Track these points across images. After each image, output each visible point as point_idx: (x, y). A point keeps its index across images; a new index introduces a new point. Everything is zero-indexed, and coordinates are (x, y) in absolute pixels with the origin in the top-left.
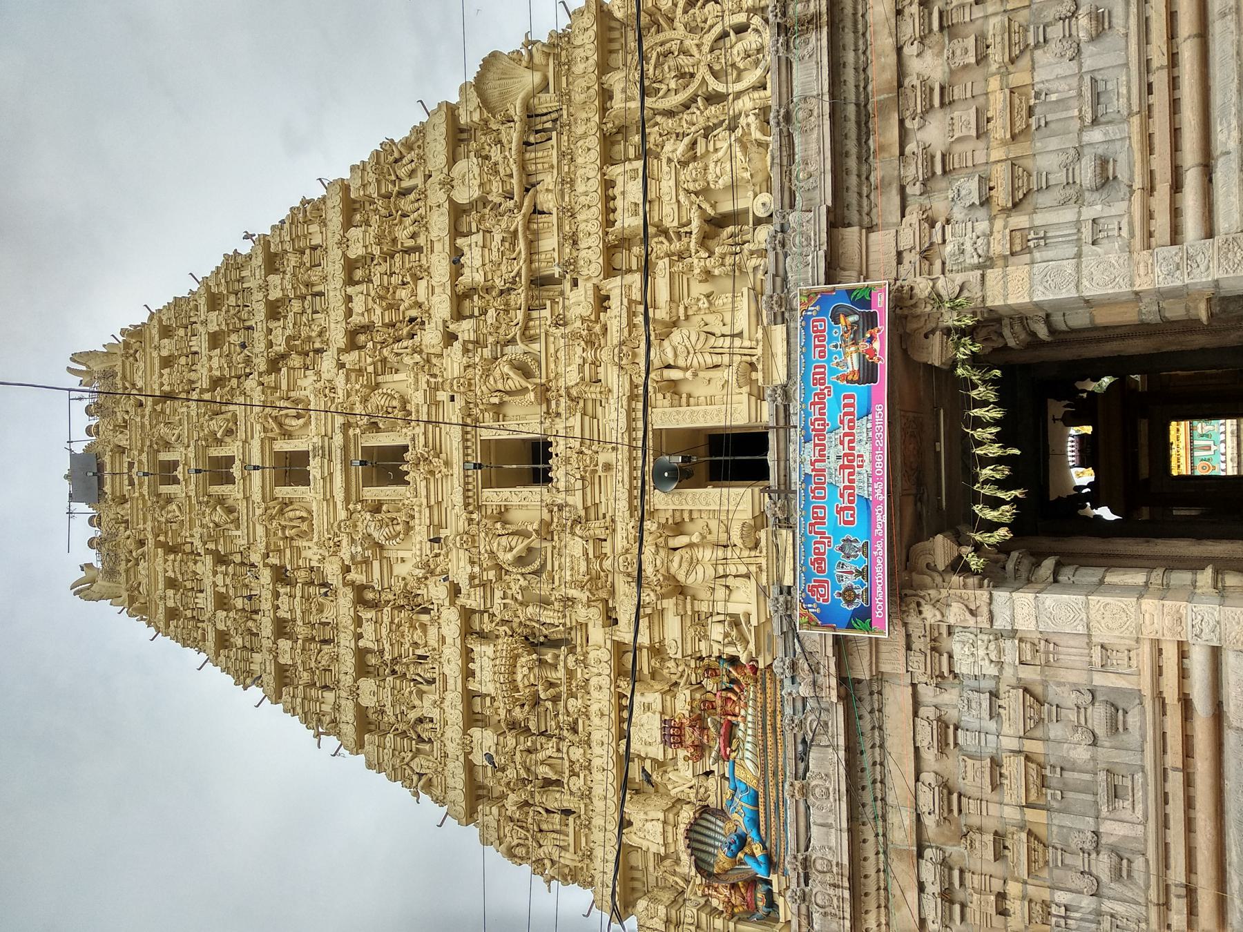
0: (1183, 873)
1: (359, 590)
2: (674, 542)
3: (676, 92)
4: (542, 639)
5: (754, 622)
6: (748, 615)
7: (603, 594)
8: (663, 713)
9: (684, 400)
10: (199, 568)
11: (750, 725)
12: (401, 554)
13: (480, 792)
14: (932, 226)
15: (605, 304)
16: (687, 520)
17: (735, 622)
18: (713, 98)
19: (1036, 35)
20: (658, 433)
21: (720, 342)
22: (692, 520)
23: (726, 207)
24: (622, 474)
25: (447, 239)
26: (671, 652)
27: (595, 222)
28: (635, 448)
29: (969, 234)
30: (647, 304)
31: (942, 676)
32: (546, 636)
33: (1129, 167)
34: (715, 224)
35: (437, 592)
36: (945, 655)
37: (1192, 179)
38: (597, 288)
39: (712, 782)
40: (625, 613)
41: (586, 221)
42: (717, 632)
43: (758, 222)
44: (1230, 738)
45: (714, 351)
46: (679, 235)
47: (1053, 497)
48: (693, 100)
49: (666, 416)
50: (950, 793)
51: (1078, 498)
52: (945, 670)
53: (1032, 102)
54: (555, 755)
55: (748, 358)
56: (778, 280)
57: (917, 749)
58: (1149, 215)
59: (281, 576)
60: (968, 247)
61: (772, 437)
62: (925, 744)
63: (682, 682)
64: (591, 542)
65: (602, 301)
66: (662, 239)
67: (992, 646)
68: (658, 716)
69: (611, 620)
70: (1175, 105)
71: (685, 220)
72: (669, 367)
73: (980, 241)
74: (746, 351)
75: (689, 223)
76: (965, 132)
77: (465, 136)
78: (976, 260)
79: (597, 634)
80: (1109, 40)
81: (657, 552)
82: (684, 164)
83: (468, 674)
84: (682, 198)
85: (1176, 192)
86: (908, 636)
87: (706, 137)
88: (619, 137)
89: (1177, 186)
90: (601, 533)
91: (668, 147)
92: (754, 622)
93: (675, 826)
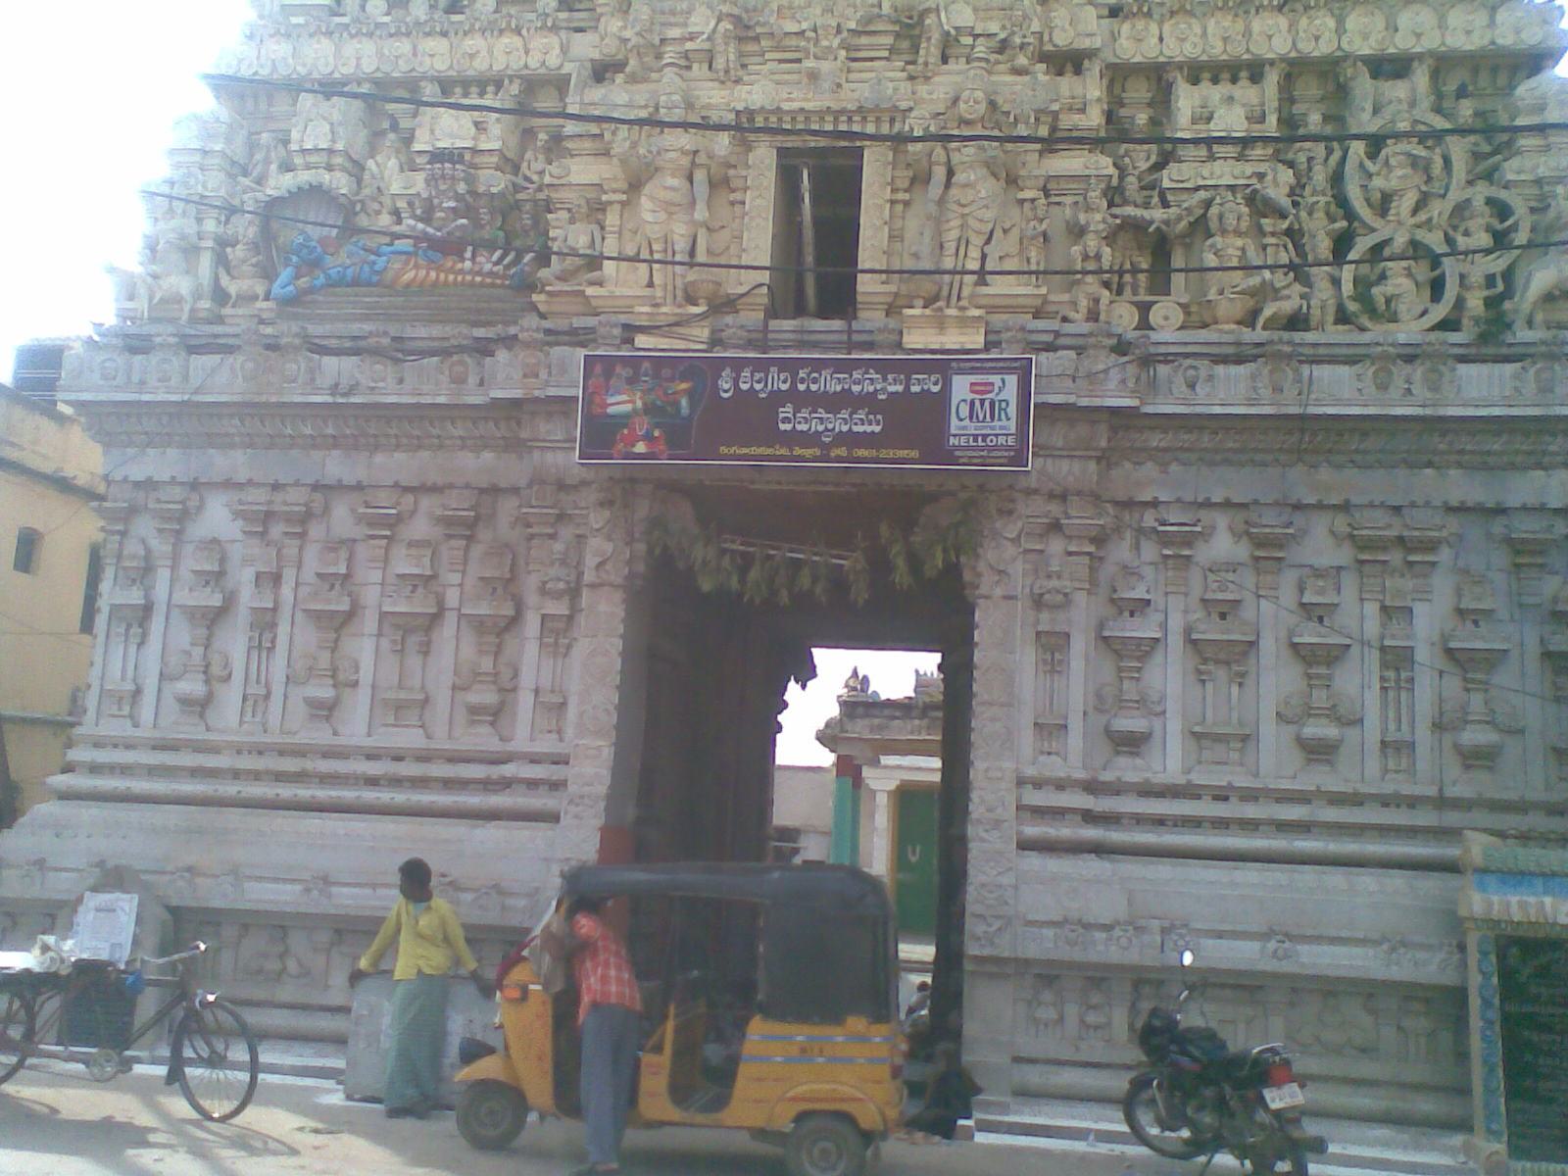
0: (1034, 803)
2: (700, 176)
3: (1364, 187)
5: (590, 291)
6: (600, 284)
7: (633, 63)
8: (475, 151)
9: (901, 196)
11: (460, 278)
14: (1093, 540)
16: (732, 197)
17: (594, 262)
20: (859, 153)
21: (975, 253)
22: (732, 203)
23: (1178, 260)
24: (798, 98)
26: (554, 169)
27: (1198, 50)
28: (836, 121)
30: (1051, 144)
33: (1128, 770)
36: (550, 531)
38: (1091, 54)
39: (385, 220)
40: (617, 96)
41: (1204, 33)
42: (579, 237)
43: (1144, 309)
45: (963, 242)
46: (1152, 186)
48: (1350, 215)
49: (875, 168)
50: (390, 526)
52: (535, 530)
55: (945, 293)
56: (1048, 338)
58: (1060, 786)
60: (1054, 583)
61: (837, 324)
63: (520, 181)
64: (707, 46)
65: (1067, 62)
66: (1153, 158)
67: (561, 585)
68: (469, 144)
69: (602, 71)
71: (1170, 197)
72: (950, 173)
73: (1060, 598)
74: (955, 292)
75: (1165, 204)
79: (587, 47)
80: (1296, 757)
81: (684, 152)
82: (1251, 200)
84: (1203, 194)
85: (1213, 823)
89: (1089, 817)
90: (720, 63)
91: (1287, 176)
92: (590, 291)
93: (330, 168)
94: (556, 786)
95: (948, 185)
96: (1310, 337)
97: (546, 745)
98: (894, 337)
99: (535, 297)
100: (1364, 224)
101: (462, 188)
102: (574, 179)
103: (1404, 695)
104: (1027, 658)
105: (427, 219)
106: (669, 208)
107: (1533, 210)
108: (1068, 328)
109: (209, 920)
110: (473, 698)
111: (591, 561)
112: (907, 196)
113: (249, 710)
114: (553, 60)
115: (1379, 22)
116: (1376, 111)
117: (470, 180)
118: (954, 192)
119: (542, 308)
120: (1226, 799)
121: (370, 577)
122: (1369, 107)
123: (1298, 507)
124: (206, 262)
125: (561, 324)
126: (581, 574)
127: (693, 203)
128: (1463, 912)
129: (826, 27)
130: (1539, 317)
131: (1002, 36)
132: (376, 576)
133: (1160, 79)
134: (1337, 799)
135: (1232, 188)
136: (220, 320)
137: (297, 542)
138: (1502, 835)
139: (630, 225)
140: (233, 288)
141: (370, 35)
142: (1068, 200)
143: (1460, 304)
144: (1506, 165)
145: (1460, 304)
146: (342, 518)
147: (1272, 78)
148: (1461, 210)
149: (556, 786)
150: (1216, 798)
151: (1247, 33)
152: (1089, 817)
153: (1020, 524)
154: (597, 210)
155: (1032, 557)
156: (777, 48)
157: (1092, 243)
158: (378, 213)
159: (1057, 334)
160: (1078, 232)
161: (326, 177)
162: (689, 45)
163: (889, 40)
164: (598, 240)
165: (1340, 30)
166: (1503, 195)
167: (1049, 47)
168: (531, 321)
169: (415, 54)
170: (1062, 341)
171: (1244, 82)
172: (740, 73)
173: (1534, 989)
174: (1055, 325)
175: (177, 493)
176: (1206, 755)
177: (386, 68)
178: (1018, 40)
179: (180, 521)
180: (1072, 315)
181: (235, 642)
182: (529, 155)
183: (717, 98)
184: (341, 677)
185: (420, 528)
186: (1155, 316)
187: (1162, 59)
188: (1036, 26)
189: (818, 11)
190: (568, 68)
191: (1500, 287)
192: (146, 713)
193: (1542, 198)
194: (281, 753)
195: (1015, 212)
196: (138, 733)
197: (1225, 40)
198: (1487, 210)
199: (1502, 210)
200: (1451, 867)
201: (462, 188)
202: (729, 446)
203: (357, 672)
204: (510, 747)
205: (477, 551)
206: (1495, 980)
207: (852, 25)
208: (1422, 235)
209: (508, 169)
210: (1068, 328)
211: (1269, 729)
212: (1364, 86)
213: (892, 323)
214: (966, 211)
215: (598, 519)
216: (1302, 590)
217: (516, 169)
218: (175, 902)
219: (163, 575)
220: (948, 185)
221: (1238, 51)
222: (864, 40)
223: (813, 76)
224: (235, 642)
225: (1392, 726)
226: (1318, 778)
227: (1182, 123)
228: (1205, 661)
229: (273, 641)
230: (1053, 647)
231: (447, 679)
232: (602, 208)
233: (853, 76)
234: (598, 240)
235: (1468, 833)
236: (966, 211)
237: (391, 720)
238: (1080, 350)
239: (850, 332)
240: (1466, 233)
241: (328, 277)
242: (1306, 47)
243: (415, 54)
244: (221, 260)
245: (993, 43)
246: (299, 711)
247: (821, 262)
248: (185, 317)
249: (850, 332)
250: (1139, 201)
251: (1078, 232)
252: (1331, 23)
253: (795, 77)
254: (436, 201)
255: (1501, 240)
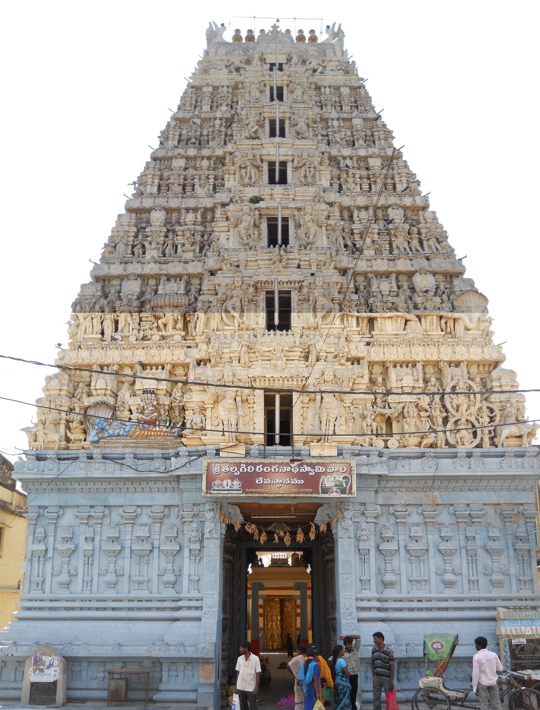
1: (212, 210)
4: (188, 319)
7: (213, 361)
8: (157, 389)
9: (306, 405)
10: (224, 108)
12: (231, 238)
13: (107, 283)
14: (375, 518)
15: (356, 362)
16: (249, 406)
18: (446, 421)
19: (448, 560)
25: (395, 269)
29: (369, 533)
31: (183, 518)
32: (189, 321)
33: (390, 593)
34: (389, 421)
35: (212, 263)
37: (382, 615)
39: (127, 413)
43: (386, 441)
44: (166, 624)
47: (257, 553)
48: (447, 411)
51: (254, 560)
53: (421, 558)
54: (131, 327)
56: (358, 452)
57: (150, 506)
59: (221, 160)
61: (289, 448)
62: (153, 510)
65: (356, 361)
70: (412, 609)
71: (391, 405)
73: (366, 537)
75: (390, 408)
76: (412, 531)
77: (448, 279)
78: (358, 535)
80: (442, 586)
82: (417, 406)
83: (169, 278)
86: (199, 504)
87: (428, 417)
88: (436, 369)
89: (379, 609)
90: (242, 361)
92: (202, 438)
93: (105, 395)
94: (201, 608)
95: (322, 402)
96: (439, 450)
97: (194, 594)
98: (308, 453)
99: (183, 440)
100: (452, 414)
101: (155, 403)
102: (194, 400)
103: (474, 564)
104: (354, 558)
105: (142, 413)
106: (229, 410)
107: (500, 410)
108: (363, 448)
109: (77, 660)
110: (164, 578)
111: (207, 531)
112: (308, 406)
113: (85, 585)
114: (182, 358)
115: (450, 349)
116: (452, 379)
117: (157, 400)
118: (324, 404)
119: (185, 443)
120: (421, 601)
121: (127, 538)
122: (450, 377)
123: (437, 505)
124: (62, 428)
125: (193, 449)
126: (203, 535)
127: (237, 408)
128: (498, 633)
129: (278, 350)
130: (505, 444)
131: (336, 353)
132: (128, 537)
133: (384, 366)
134: (456, 600)
135: (410, 402)
136: (68, 448)
137: (100, 526)
138: (507, 608)
139: (215, 415)
140: (72, 437)
141: (117, 348)
142: (360, 407)
143: (482, 439)
144: (491, 396)
145: (482, 439)
146: (115, 516)
147: (419, 366)
148: (480, 409)
149: (201, 608)
150: (418, 601)
151: (411, 352)
152: (379, 609)
153: (352, 513)
154: (203, 410)
155: (356, 524)
156: (262, 356)
157: (369, 420)
158: (123, 411)
159: (360, 450)
160: (364, 417)
161: (105, 399)
162: (232, 355)
163: (299, 354)
164: (204, 420)
165: (439, 353)
166: (491, 406)
167: (349, 356)
168: (183, 448)
169: (133, 355)
170: (361, 453)
171: (404, 368)
172: (250, 364)
173: (520, 656)
174: (359, 447)
175: (54, 510)
176: (414, 587)
177: (123, 360)
178: (341, 355)
179: (56, 519)
180: (364, 444)
181: (79, 561)
182: (175, 390)
183: (243, 374)
184: (118, 573)
185: (144, 519)
186: (389, 444)
187: (385, 360)
188: (346, 350)
189: (275, 344)
190: (188, 360)
191: (493, 434)
192: (95, 588)
193: (503, 406)
194: (113, 601)
195: (343, 410)
196: (92, 596)
197: (404, 354)
198: (487, 410)
199: (491, 410)
200: (493, 619)
201: (155, 403)
202: (249, 488)
203: (123, 570)
204: (181, 595)
205: (164, 527)
206: (508, 654)
207: (287, 349)
208: (469, 418)
209: (168, 395)
210: (363, 448)
211: (433, 577)
212: (448, 371)
213: (307, 448)
214: (328, 411)
215: (209, 515)
216: (440, 532)
217: (170, 395)
218: (64, 655)
219: (51, 540)
220: (322, 402)
221: (408, 358)
222: (290, 354)
223: (275, 366)
224: (79, 561)
225: (471, 575)
226: (449, 593)
227: (393, 383)
228: (412, 556)
229: (93, 561)
230: (363, 555)
231: (156, 572)
232: (205, 409)
233: (288, 366)
234: (204, 420)
235: (499, 609)
236: (328, 411)
237: (136, 587)
238: (368, 456)
239: (293, 450)
240: (482, 417)
241: (109, 434)
242: (429, 358)
243: (133, 355)
244: (68, 427)
245: (333, 355)
246: (55, 587)
247: (279, 428)
248: (57, 447)
249: (293, 450)
250: (382, 406)
251: (364, 417)
252: (436, 350)
253: (269, 366)
254: (145, 407)
255: (492, 419)
